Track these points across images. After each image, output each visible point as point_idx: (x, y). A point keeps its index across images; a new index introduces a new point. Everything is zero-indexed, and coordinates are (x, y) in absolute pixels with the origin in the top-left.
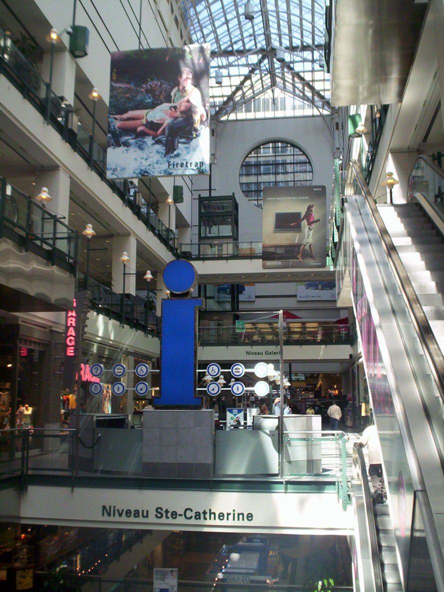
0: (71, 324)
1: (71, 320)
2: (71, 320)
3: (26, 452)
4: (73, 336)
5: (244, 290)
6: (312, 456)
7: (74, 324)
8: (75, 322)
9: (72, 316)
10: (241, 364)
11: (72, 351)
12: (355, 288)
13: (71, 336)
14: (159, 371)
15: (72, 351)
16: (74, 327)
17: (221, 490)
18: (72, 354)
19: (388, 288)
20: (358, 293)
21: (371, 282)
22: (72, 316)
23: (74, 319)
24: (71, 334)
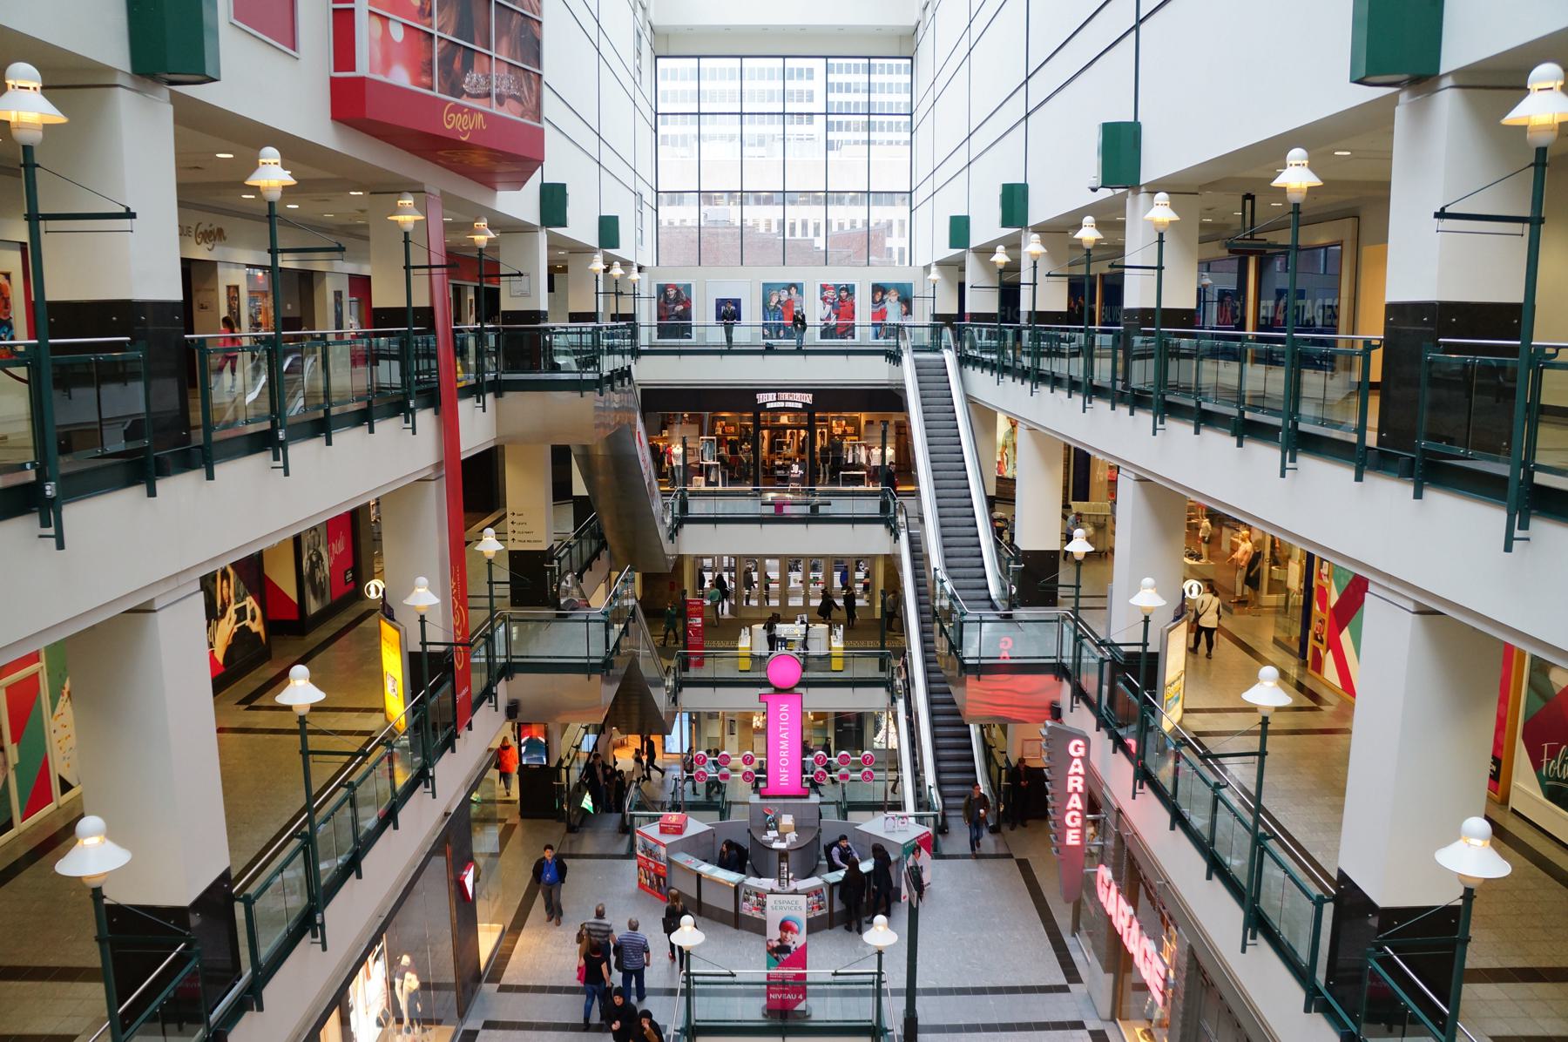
0: (1075, 789)
1: (1076, 782)
2: (1076, 782)
3: (33, 299)
4: (1079, 811)
5: (311, 680)
6: (811, 996)
7: (1080, 789)
8: (1084, 785)
9: (1076, 774)
10: (263, 379)
11: (1077, 837)
12: (1120, 986)
13: (1075, 809)
14: (36, 341)
15: (1077, 837)
16: (1080, 794)
17: (694, 737)
18: (1077, 843)
19: (304, 653)
20: (978, 619)
21: (1337, 1032)
22: (1076, 774)
23: (1080, 780)
24: (1074, 806)
